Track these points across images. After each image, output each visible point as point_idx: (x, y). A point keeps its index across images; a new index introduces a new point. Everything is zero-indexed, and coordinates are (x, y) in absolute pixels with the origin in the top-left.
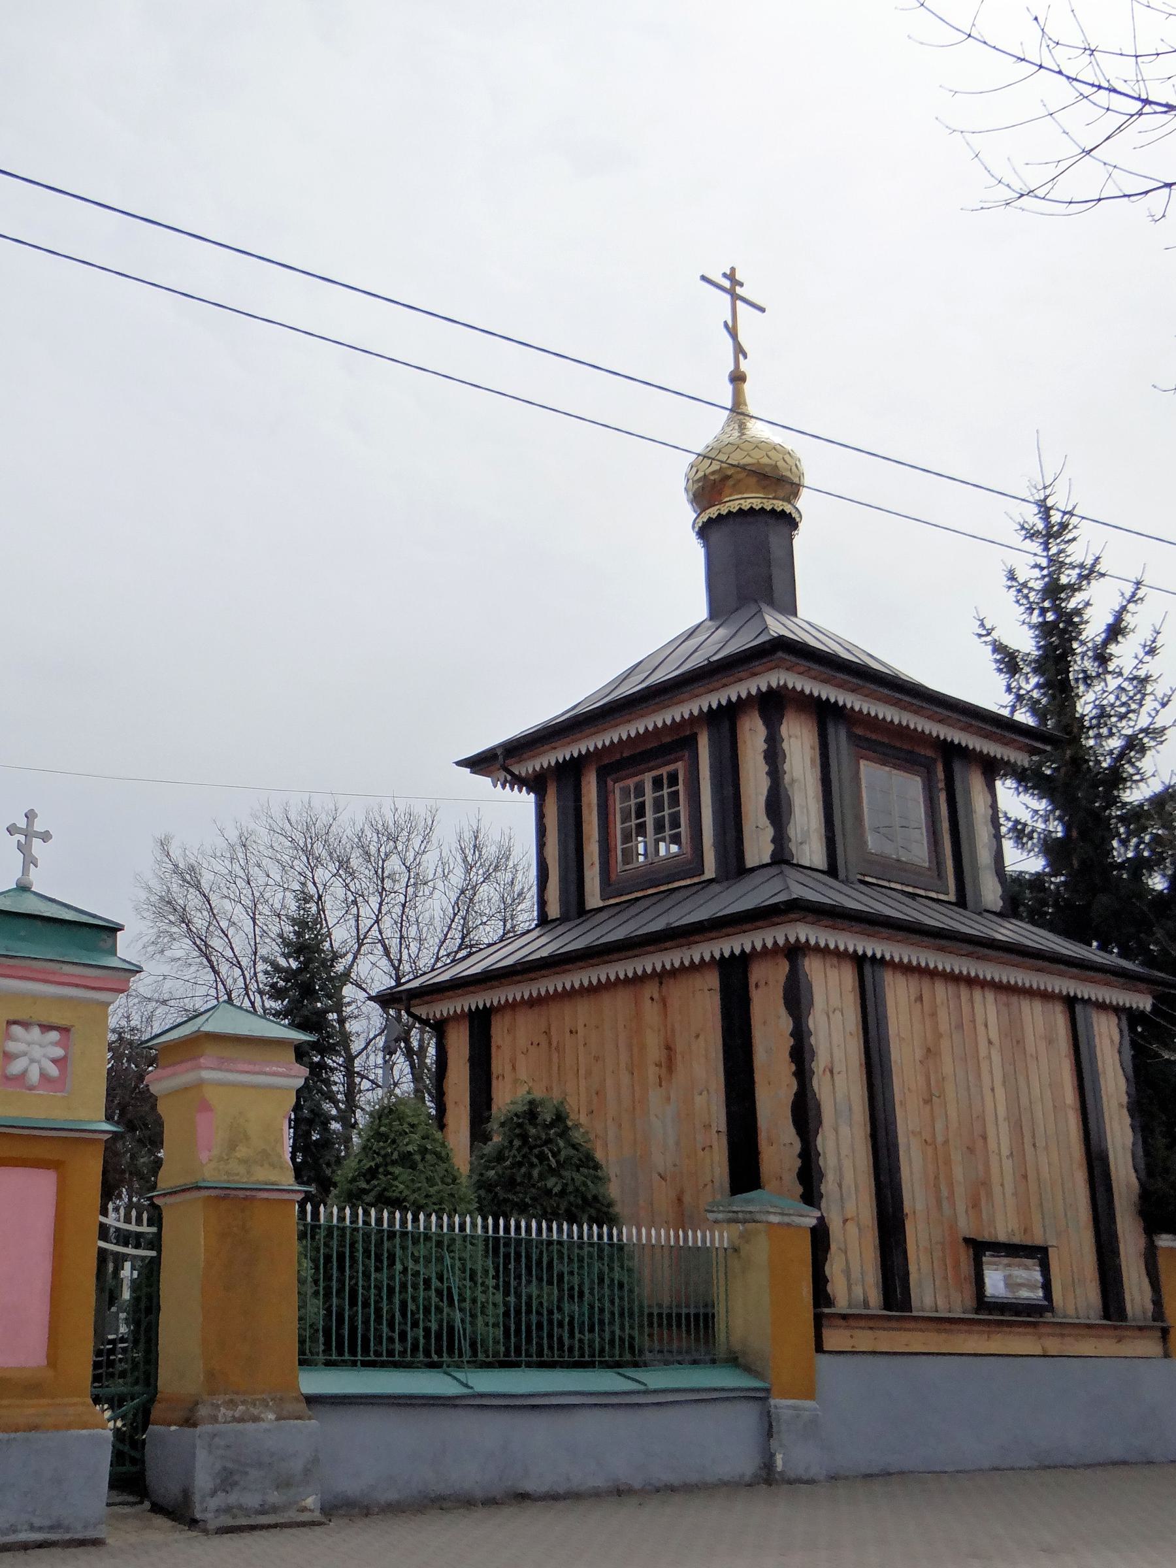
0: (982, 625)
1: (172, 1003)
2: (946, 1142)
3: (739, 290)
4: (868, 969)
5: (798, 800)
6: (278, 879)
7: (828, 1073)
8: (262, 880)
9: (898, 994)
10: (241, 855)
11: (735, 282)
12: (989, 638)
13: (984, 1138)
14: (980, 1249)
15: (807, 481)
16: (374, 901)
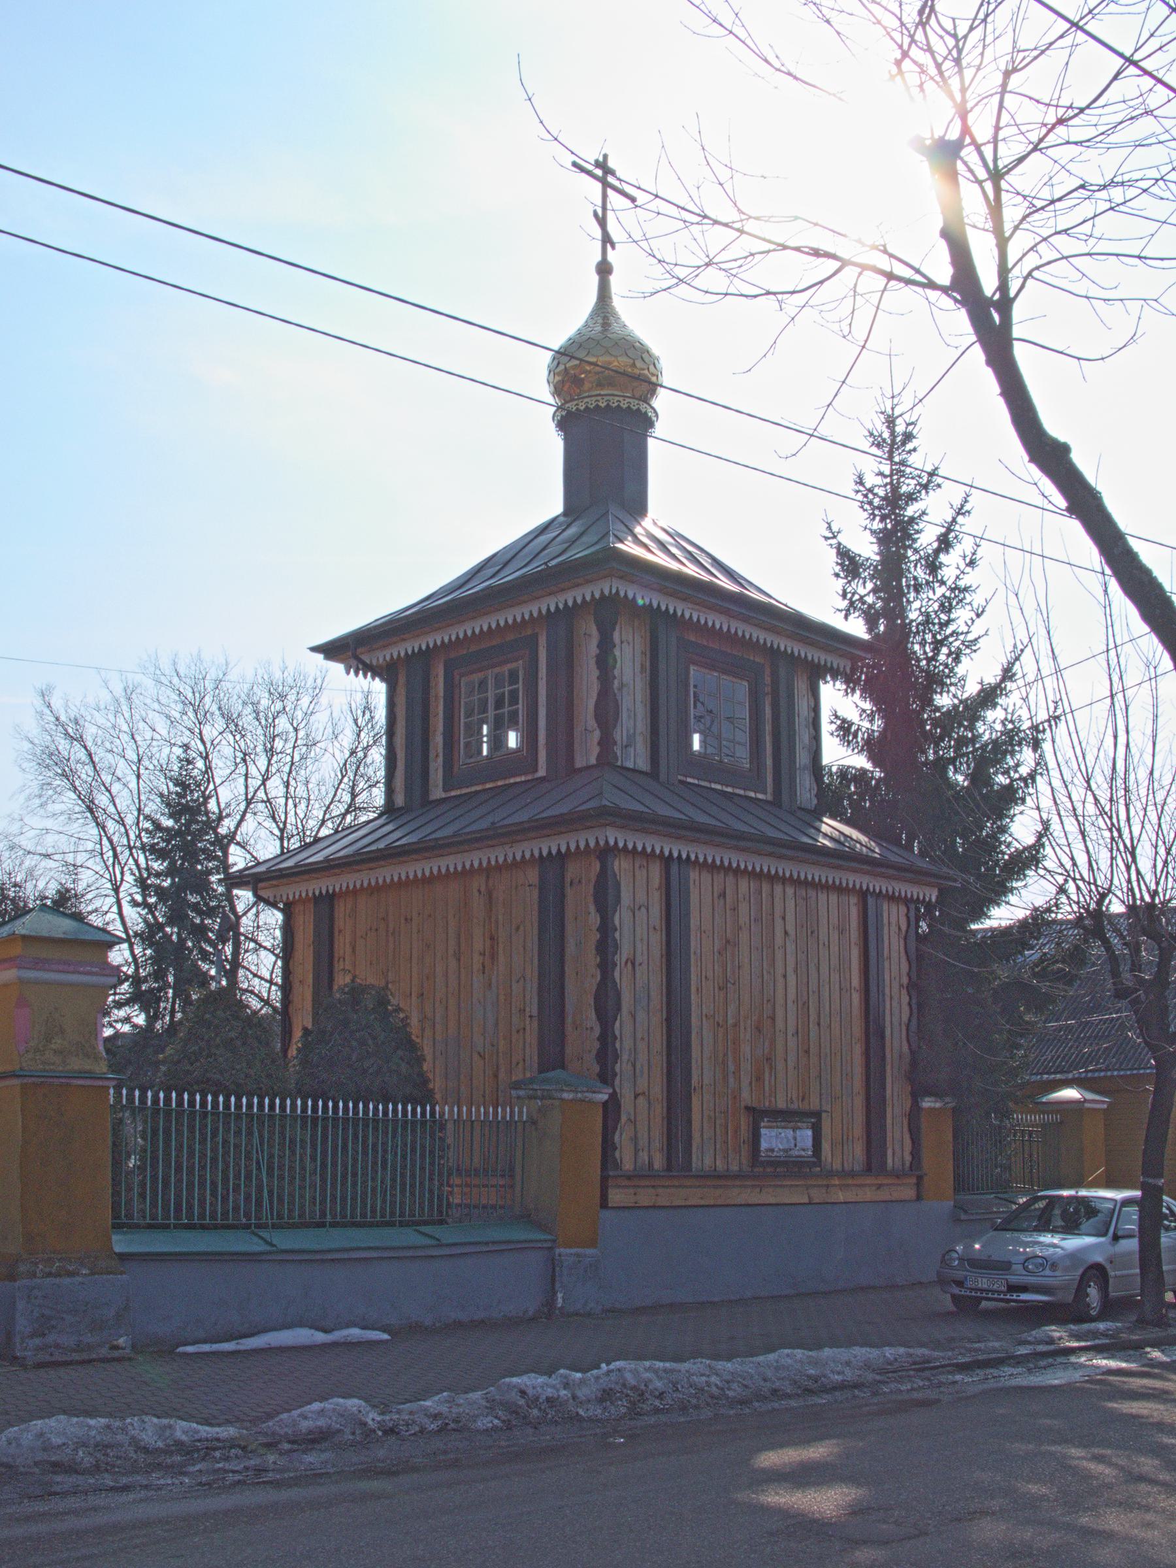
0: (829, 528)
1: (56, 857)
2: (736, 1025)
3: (610, 179)
4: (674, 869)
5: (626, 703)
6: (164, 733)
7: (629, 964)
8: (148, 734)
9: (701, 890)
10: (125, 708)
11: (608, 171)
12: (834, 542)
13: (773, 1019)
14: (758, 1115)
15: (666, 380)
16: (262, 762)
